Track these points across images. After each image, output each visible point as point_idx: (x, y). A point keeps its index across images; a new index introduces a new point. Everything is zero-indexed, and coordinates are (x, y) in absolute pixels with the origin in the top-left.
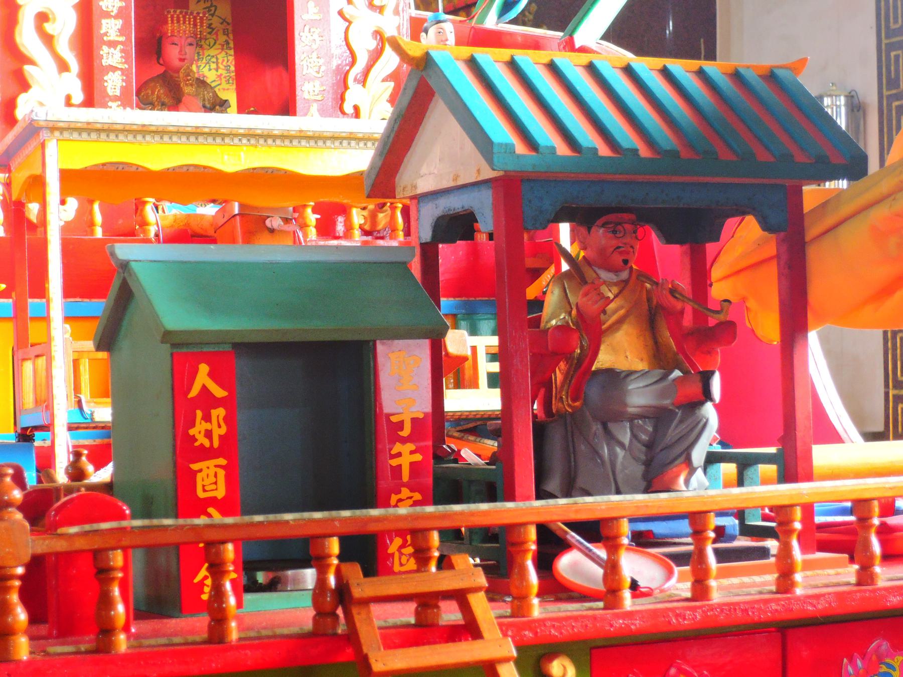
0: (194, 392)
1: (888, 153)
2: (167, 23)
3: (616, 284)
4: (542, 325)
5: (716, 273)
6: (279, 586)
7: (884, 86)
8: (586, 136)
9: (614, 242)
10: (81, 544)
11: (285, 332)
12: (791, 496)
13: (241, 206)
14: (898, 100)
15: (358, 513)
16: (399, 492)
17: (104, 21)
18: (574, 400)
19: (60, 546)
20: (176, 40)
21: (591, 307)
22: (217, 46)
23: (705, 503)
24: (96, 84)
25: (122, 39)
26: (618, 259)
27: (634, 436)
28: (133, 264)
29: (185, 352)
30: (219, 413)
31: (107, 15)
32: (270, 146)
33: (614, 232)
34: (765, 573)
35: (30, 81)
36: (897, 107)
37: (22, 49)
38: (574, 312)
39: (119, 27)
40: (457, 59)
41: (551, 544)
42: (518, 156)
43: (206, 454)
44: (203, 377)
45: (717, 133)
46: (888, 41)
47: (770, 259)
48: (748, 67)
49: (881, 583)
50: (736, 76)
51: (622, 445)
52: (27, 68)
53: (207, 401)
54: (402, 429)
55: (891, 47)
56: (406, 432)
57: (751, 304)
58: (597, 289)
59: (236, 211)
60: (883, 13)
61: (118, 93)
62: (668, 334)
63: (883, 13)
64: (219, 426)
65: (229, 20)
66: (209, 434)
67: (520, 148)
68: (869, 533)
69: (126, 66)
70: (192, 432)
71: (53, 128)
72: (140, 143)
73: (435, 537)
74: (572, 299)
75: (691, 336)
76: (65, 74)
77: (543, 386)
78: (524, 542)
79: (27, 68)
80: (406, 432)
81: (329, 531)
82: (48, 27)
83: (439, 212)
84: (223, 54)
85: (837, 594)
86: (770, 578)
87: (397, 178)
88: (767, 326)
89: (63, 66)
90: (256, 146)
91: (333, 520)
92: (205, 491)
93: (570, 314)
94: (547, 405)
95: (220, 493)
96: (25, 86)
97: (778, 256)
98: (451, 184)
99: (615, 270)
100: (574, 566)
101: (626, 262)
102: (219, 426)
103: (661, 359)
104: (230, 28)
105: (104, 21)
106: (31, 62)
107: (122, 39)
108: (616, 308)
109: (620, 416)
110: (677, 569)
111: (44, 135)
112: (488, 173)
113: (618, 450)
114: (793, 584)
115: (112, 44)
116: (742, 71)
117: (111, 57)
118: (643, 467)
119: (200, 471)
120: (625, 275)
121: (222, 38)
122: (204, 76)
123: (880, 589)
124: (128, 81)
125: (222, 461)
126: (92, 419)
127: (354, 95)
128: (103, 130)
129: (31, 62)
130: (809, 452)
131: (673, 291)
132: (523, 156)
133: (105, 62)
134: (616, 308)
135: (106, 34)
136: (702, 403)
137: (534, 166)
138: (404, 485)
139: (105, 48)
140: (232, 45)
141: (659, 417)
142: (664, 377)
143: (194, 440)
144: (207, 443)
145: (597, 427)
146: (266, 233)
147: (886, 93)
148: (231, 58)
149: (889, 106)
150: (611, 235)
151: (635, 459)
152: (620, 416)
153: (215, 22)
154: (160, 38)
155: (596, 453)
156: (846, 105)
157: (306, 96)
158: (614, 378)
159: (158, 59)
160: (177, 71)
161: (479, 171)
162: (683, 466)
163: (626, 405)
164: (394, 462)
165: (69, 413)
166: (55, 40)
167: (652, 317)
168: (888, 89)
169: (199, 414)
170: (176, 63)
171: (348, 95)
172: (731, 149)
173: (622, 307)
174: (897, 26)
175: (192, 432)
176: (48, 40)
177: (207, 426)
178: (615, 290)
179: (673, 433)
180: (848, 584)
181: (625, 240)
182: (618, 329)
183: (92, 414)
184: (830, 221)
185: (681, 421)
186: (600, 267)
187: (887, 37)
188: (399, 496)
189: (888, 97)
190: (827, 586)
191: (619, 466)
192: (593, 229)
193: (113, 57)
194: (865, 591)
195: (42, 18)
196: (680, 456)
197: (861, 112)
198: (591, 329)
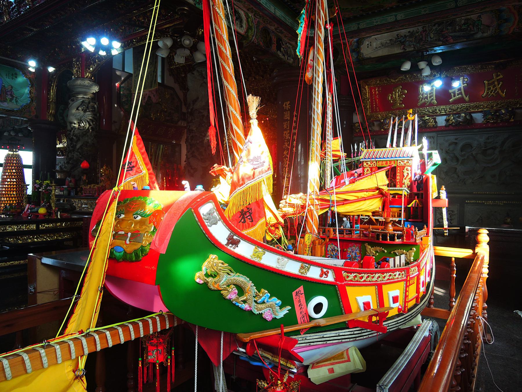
127: (404, 181)
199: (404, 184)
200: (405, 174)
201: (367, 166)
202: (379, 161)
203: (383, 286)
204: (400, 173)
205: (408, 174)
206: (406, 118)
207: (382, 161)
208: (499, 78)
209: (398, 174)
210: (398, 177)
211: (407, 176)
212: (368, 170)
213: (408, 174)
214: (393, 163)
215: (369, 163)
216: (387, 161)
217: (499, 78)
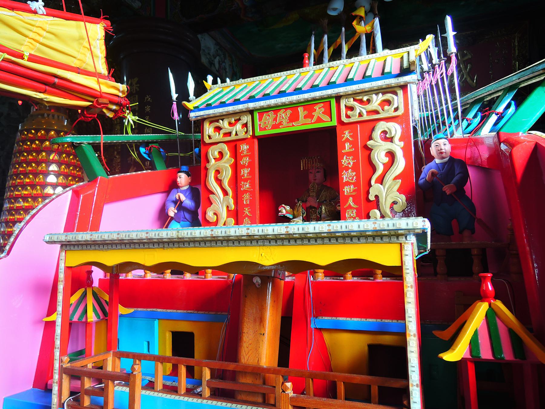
89: (225, 193)
127: (376, 189)
129: (212, 193)
176: (219, 182)
200: (380, 158)
201: (218, 137)
202: (263, 111)
204: (354, 154)
205: (391, 155)
206: (351, 32)
207: (276, 109)
208: (466, 58)
209: (345, 161)
210: (346, 176)
211: (388, 166)
212: (221, 154)
213: (391, 155)
214: (319, 111)
217: (466, 58)
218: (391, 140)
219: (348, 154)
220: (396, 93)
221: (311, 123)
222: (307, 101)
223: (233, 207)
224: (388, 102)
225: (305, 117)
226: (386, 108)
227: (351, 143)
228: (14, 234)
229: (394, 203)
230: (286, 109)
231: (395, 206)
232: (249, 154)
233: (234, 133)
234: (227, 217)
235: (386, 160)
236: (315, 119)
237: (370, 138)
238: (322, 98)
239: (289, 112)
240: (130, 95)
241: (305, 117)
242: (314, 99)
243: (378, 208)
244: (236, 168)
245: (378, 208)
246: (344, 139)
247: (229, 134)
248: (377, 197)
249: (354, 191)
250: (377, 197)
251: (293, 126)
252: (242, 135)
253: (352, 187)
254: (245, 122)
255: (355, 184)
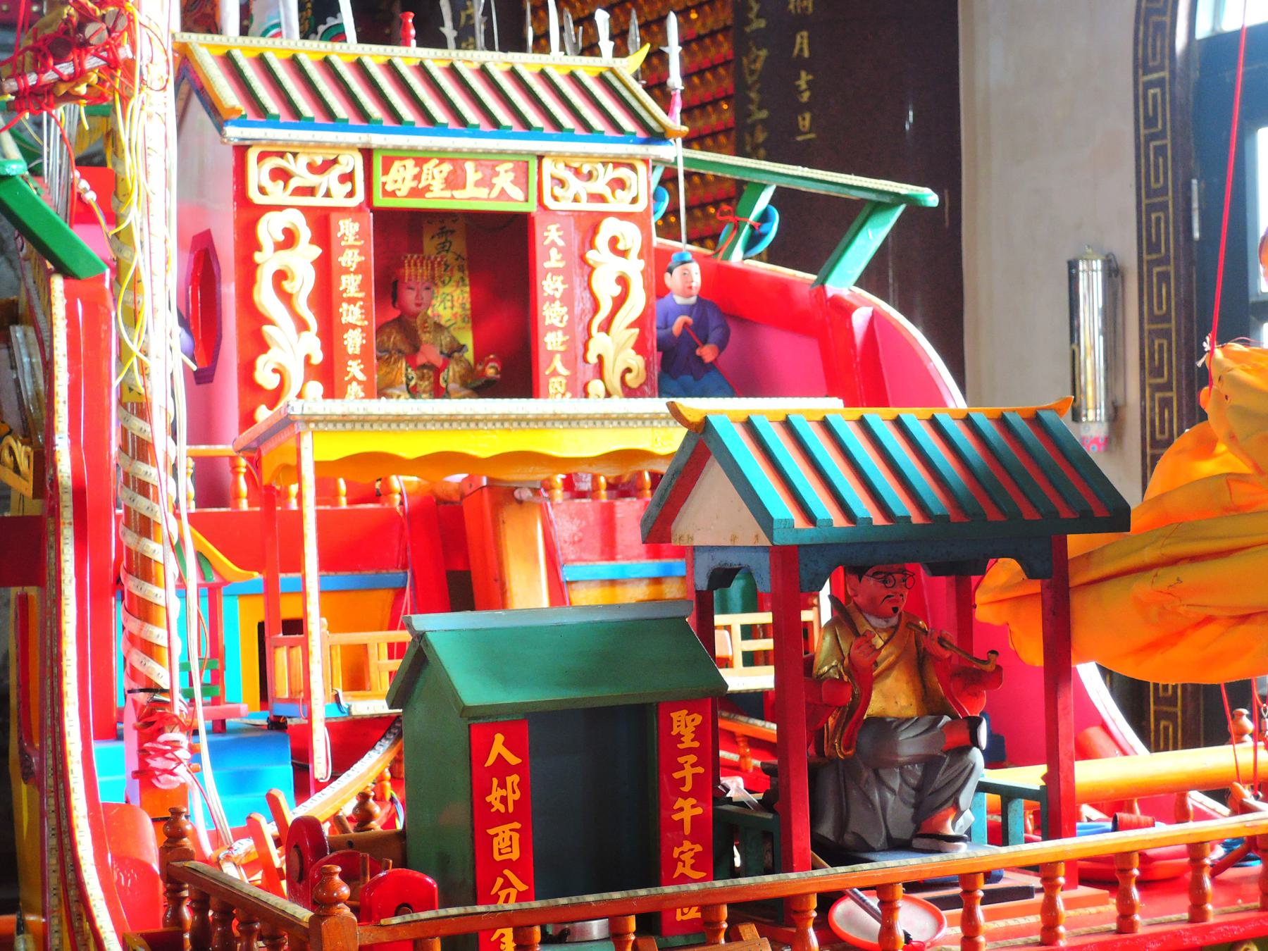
0: (490, 762)
1: (1152, 471)
2: (403, 266)
3: (884, 630)
4: (815, 671)
5: (980, 597)
6: (568, 939)
7: (1146, 321)
8: (862, 506)
9: (884, 592)
10: (404, 934)
11: (576, 700)
12: (1056, 854)
13: (489, 480)
14: (1158, 265)
15: (653, 891)
16: (682, 845)
17: (343, 278)
18: (847, 749)
19: (384, 937)
20: (412, 285)
21: (862, 658)
22: (452, 283)
23: (973, 865)
24: (336, 343)
25: (361, 295)
26: (888, 607)
27: (904, 780)
28: (429, 635)
29: (481, 724)
30: (513, 779)
31: (346, 271)
32: (523, 429)
33: (885, 582)
34: (1029, 914)
35: (269, 342)
36: (1158, 274)
37: (261, 309)
38: (846, 662)
39: (358, 282)
40: (734, 422)
41: (828, 900)
42: (797, 530)
43: (504, 819)
44: (498, 746)
45: (986, 490)
46: (1149, 201)
47: (1036, 594)
48: (1014, 411)
49: (1140, 931)
50: (1002, 422)
51: (892, 791)
52: (266, 329)
53: (502, 768)
54: (684, 785)
55: (1151, 208)
56: (687, 788)
57: (1013, 628)
58: (869, 641)
59: (484, 483)
60: (1143, 170)
61: (357, 351)
62: (936, 679)
63: (1143, 170)
64: (514, 792)
65: (464, 255)
66: (504, 800)
67: (799, 523)
68: (1130, 883)
69: (366, 323)
70: (488, 799)
71: (308, 420)
72: (394, 432)
73: (725, 911)
74: (845, 646)
75: (958, 676)
76: (304, 334)
77: (818, 737)
78: (806, 911)
79: (266, 329)
80: (687, 788)
81: (628, 911)
82: (287, 285)
83: (715, 565)
84: (458, 291)
85: (1099, 944)
86: (1035, 919)
87: (674, 525)
88: (1032, 652)
89: (302, 326)
90: (509, 430)
91: (631, 899)
92: (500, 854)
93: (842, 662)
94: (820, 752)
95: (515, 855)
96: (263, 347)
97: (1042, 594)
98: (729, 543)
99: (885, 617)
100: (848, 916)
101: (895, 610)
102: (514, 792)
103: (931, 705)
104: (465, 264)
105: (343, 278)
106: (270, 322)
107: (361, 295)
108: (887, 655)
109: (891, 764)
110: (944, 913)
111: (300, 427)
112: (764, 541)
113: (889, 795)
114: (1057, 936)
115: (352, 301)
116: (1008, 415)
117: (351, 314)
118: (912, 810)
119: (497, 835)
120: (894, 621)
121: (457, 275)
122: (439, 316)
123: (1140, 937)
124: (367, 338)
125: (517, 825)
126: (349, 713)
127: (600, 344)
128: (358, 421)
129: (270, 322)
130: (1071, 770)
131: (941, 641)
132: (802, 530)
133: (344, 320)
134: (887, 655)
135: (345, 290)
136: (969, 749)
137: (812, 539)
138: (686, 838)
139: (345, 305)
140: (467, 281)
141: (930, 763)
142: (933, 725)
143: (491, 805)
144: (502, 809)
145: (867, 774)
146: (515, 505)
147: (1145, 257)
148: (467, 295)
149: (1147, 147)
150: (880, 584)
151: (905, 802)
152: (891, 764)
153: (450, 257)
154: (396, 283)
155: (868, 800)
156: (1103, 270)
157: (549, 348)
158: (885, 727)
159: (394, 304)
160: (415, 315)
161: (757, 536)
162: (951, 810)
163: (897, 755)
164: (676, 817)
165: (327, 709)
166: (294, 299)
167: (919, 664)
168: (1149, 253)
169: (495, 781)
170: (413, 308)
171: (591, 344)
172: (999, 508)
173: (891, 654)
174: (1158, 186)
175: (488, 799)
176: (286, 298)
177: (503, 792)
178: (885, 636)
179: (940, 779)
180: (1109, 931)
181: (894, 590)
182: (888, 676)
183: (349, 708)
184: (1094, 574)
185: (949, 766)
186: (870, 614)
187: (1148, 197)
188: (681, 849)
189: (1149, 262)
190: (1089, 934)
191: (889, 811)
192: (864, 578)
193: (354, 315)
194: (1125, 940)
195: (280, 276)
196: (947, 801)
197: (1119, 278)
198: (862, 677)
199: (599, 370)
200: (606, 290)
201: (277, 193)
203: (102, 799)
205: (623, 281)
211: (619, 302)
212: (289, 239)
213: (623, 281)
214: (505, 178)
215: (298, 167)
216: (456, 159)
218: (623, 254)
219: (556, 272)
220: (633, 168)
221: (488, 199)
222: (488, 152)
223: (318, 358)
224: (619, 184)
225: (478, 184)
226: (618, 192)
227: (560, 250)
228: (212, 447)
229: (628, 370)
230: (442, 161)
231: (628, 377)
232: (358, 243)
233: (322, 191)
234: (306, 380)
235: (617, 290)
236: (495, 192)
237: (592, 246)
238: (516, 153)
239: (447, 167)
240: (671, 335)
241: (478, 184)
242: (501, 152)
243: (601, 377)
244: (326, 269)
245: (601, 377)
246: (546, 243)
247: (311, 191)
248: (600, 357)
249: (563, 343)
250: (600, 357)
251: (453, 197)
252: (338, 200)
253: (560, 333)
254: (348, 170)
255: (566, 331)
